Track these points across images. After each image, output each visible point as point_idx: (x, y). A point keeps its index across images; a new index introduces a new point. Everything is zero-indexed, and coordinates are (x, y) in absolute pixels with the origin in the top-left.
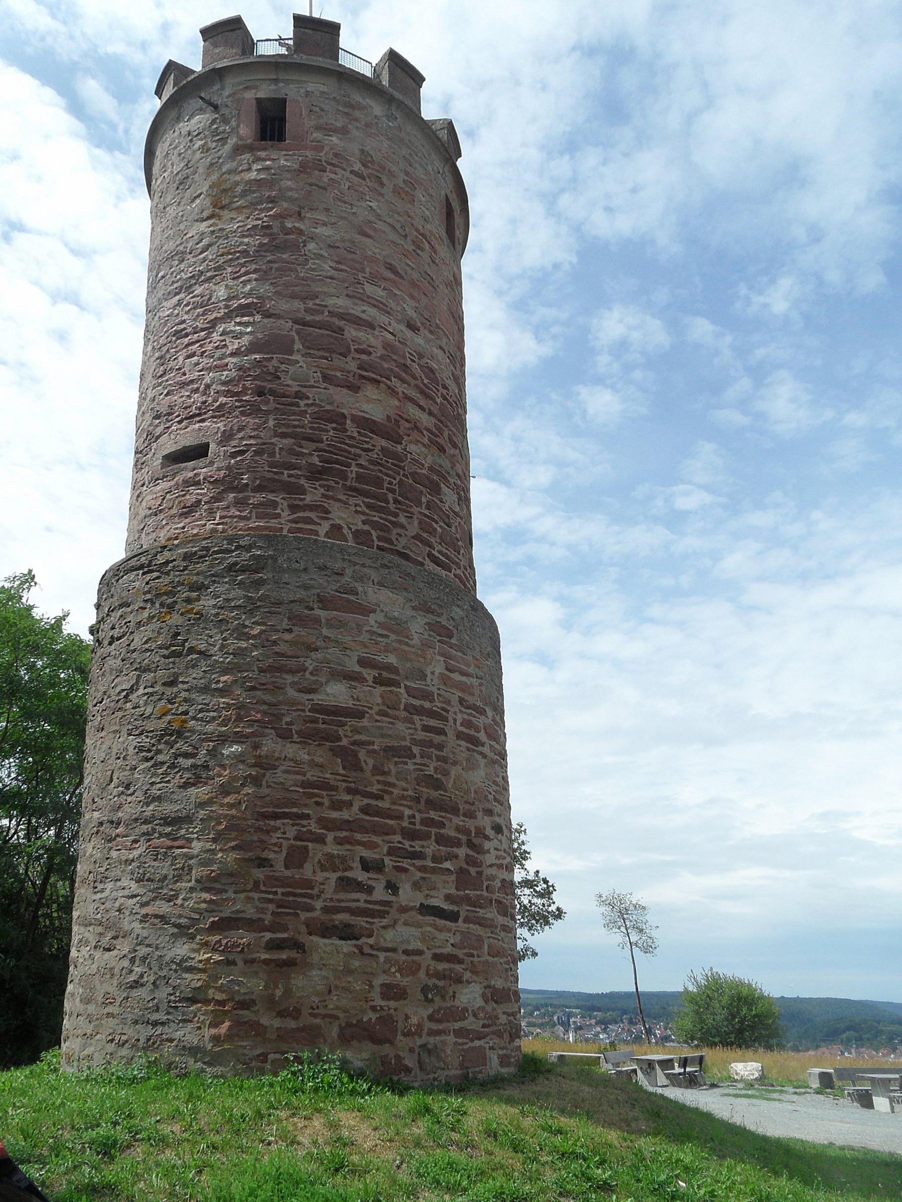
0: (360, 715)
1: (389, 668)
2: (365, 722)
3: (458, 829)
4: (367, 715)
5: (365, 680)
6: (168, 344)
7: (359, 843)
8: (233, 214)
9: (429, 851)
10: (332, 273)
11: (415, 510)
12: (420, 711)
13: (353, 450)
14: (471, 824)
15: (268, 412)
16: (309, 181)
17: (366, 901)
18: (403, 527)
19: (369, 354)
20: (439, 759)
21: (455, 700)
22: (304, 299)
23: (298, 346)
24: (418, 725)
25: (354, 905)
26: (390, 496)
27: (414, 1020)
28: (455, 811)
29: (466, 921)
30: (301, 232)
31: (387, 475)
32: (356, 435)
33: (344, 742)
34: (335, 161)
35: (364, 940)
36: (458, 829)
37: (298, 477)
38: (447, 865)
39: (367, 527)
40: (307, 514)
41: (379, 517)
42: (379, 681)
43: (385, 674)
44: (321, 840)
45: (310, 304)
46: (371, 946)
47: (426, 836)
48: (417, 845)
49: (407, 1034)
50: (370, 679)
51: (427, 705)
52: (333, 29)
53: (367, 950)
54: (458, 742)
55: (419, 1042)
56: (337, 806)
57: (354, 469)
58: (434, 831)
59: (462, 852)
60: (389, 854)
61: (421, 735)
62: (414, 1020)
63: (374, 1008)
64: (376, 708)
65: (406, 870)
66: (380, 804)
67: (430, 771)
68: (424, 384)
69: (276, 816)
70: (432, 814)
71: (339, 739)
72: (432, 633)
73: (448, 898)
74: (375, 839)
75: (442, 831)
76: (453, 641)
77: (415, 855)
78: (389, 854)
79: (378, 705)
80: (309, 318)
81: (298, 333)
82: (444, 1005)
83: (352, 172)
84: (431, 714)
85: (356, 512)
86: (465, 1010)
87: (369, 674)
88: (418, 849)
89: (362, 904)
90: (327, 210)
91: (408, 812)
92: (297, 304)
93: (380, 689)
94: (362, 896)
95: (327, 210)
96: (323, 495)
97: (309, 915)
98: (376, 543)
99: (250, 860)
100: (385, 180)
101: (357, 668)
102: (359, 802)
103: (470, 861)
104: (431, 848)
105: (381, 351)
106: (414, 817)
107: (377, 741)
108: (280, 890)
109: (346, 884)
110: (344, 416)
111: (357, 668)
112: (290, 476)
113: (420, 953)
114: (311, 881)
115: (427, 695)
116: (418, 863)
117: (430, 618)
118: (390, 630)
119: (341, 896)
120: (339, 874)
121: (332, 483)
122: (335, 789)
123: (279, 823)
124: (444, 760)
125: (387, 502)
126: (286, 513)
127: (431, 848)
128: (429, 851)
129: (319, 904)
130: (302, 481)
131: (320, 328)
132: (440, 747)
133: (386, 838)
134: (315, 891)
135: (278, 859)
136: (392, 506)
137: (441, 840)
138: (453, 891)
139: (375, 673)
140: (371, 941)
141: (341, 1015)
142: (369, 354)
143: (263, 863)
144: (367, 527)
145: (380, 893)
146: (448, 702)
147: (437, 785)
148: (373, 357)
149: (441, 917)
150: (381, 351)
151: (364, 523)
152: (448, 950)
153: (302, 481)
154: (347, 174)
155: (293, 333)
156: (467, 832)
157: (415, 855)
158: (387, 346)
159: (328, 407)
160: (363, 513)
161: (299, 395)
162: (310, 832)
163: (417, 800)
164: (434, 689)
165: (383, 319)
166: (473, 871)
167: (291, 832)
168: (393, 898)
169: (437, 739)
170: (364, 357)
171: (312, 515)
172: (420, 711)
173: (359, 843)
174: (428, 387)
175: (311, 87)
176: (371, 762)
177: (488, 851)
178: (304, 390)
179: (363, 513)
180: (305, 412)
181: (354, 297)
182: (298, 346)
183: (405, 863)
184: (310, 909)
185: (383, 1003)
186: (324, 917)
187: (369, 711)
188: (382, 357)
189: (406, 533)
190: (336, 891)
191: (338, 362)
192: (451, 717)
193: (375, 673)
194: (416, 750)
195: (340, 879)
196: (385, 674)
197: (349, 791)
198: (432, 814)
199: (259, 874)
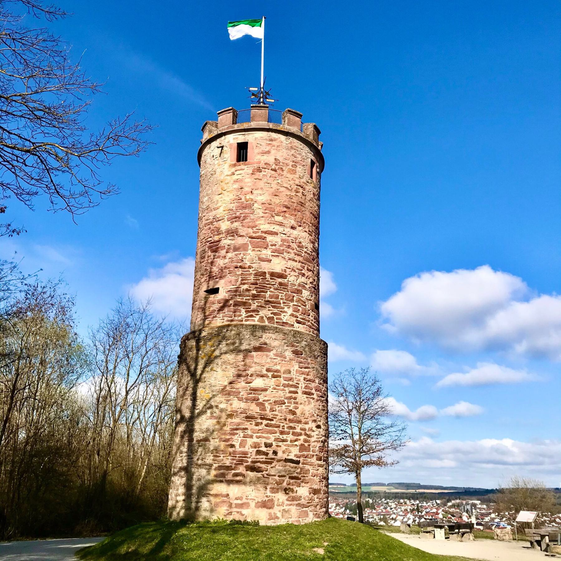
0: (266, 390)
1: (277, 371)
2: (268, 392)
3: (301, 429)
5: (268, 377)
7: (264, 437)
8: (228, 193)
9: (289, 439)
10: (263, 215)
11: (291, 304)
12: (288, 386)
13: (268, 286)
14: (307, 427)
15: (239, 275)
16: (256, 177)
17: (266, 459)
18: (286, 312)
19: (275, 245)
20: (294, 403)
21: (302, 379)
22: (252, 227)
23: (250, 247)
24: (287, 391)
25: (261, 460)
26: (282, 301)
27: (281, 501)
28: (300, 422)
29: (303, 464)
30: (252, 200)
31: (280, 293)
32: (269, 279)
33: (261, 401)
34: (265, 167)
35: (264, 472)
36: (301, 429)
37: (249, 300)
38: (296, 443)
39: (272, 315)
40: (251, 314)
42: (274, 376)
43: (275, 374)
44: (251, 437)
45: (255, 229)
46: (267, 474)
47: (288, 433)
48: (285, 437)
49: (278, 505)
50: (270, 376)
51: (291, 383)
53: (265, 476)
55: (282, 508)
56: (257, 424)
57: (269, 293)
58: (291, 431)
59: (302, 437)
60: (274, 441)
61: (289, 395)
62: (281, 501)
63: (267, 496)
64: (272, 387)
65: (280, 446)
66: (272, 422)
67: (291, 408)
69: (237, 429)
70: (291, 425)
71: (258, 399)
73: (295, 455)
74: (269, 435)
75: (295, 431)
77: (283, 441)
78: (274, 441)
80: (254, 235)
81: (250, 242)
82: (293, 495)
83: (271, 170)
84: (292, 386)
85: (269, 310)
86: (301, 497)
87: (270, 374)
88: (285, 438)
89: (264, 460)
90: (262, 188)
91: (282, 424)
92: (250, 230)
93: (274, 379)
94: (264, 457)
95: (262, 188)
96: (257, 306)
97: (246, 464)
98: (276, 320)
99: (228, 445)
100: (284, 168)
101: (265, 372)
102: (265, 422)
103: (306, 441)
104: (290, 437)
105: (280, 243)
106: (284, 426)
107: (272, 399)
108: (237, 456)
109: (259, 452)
110: (265, 273)
111: (265, 372)
112: (246, 299)
113: (284, 476)
114: (247, 452)
116: (285, 443)
117: (293, 349)
118: (277, 356)
119: (258, 457)
120: (257, 449)
121: (260, 300)
122: (257, 418)
123: (238, 432)
124: (297, 403)
125: (280, 304)
126: (245, 313)
127: (290, 437)
128: (289, 439)
129: (250, 460)
130: (250, 301)
132: (295, 398)
133: (274, 435)
134: (249, 456)
135: (237, 445)
136: (282, 305)
137: (294, 434)
138: (298, 453)
139: (272, 373)
140: (267, 472)
141: (256, 499)
142: (275, 245)
143: (232, 446)
145: (271, 455)
146: (299, 380)
147: (294, 413)
148: (277, 247)
149: (293, 463)
150: (280, 243)
151: (271, 314)
152: (295, 475)
153: (250, 301)
154: (270, 171)
155: (248, 242)
156: (304, 430)
157: (283, 441)
158: (283, 240)
159: (260, 270)
161: (250, 267)
162: (248, 434)
163: (285, 420)
164: (294, 377)
165: (280, 229)
166: (306, 444)
167: (242, 435)
168: (275, 457)
169: (294, 395)
170: (274, 247)
171: (253, 314)
172: (288, 386)
173: (264, 437)
176: (269, 407)
177: (313, 436)
178: (251, 265)
179: (271, 310)
180: (252, 273)
181: (271, 223)
182: (250, 247)
183: (280, 444)
184: (247, 462)
185: (271, 494)
186: (252, 465)
188: (280, 246)
190: (256, 455)
191: (264, 251)
192: (300, 386)
193: (272, 373)
194: (286, 401)
195: (257, 451)
196: (275, 374)
197: (261, 418)
198: (291, 425)
199: (231, 450)
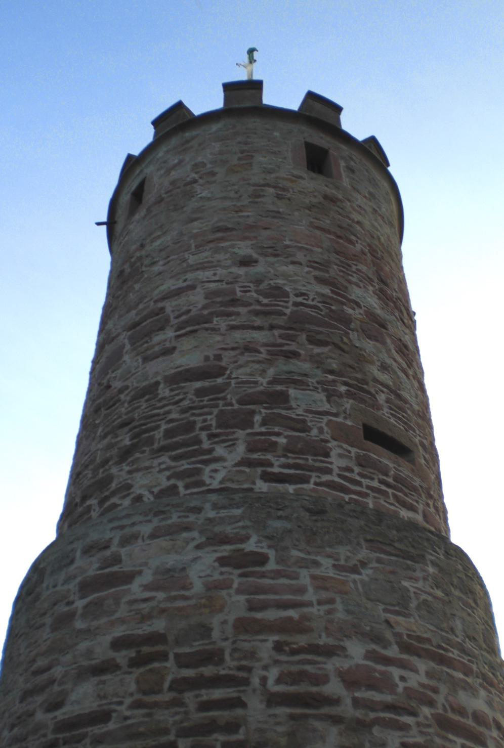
4: (114, 715)
6: (432, 423)
39: (172, 482)
41: (188, 464)
43: (145, 649)
52: (179, 106)
54: (272, 711)
64: (128, 701)
68: (266, 305)
72: (224, 569)
76: (271, 565)
79: (132, 694)
115: (213, 657)
131: (146, 320)
144: (172, 482)
151: (168, 478)
160: (168, 469)
174: (271, 305)
175: (160, 154)
187: (118, 708)
189: (225, 464)
